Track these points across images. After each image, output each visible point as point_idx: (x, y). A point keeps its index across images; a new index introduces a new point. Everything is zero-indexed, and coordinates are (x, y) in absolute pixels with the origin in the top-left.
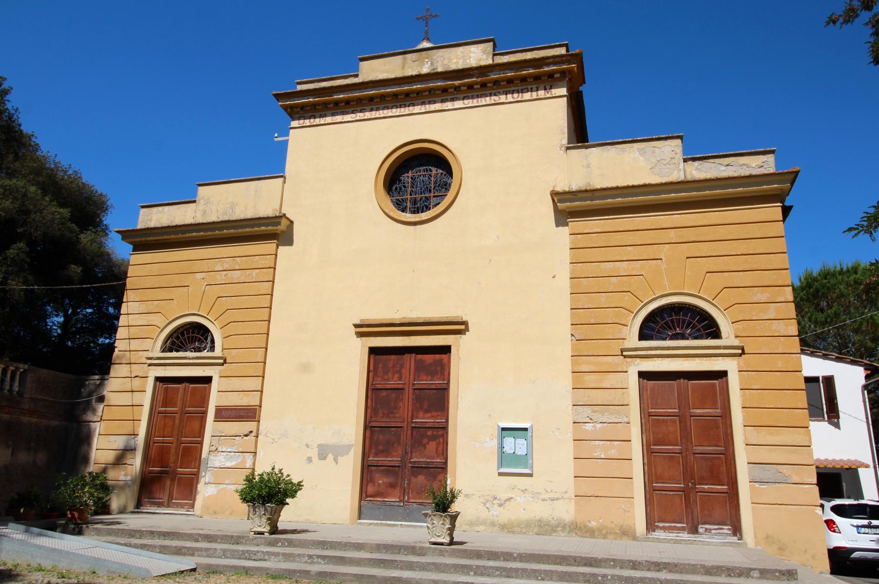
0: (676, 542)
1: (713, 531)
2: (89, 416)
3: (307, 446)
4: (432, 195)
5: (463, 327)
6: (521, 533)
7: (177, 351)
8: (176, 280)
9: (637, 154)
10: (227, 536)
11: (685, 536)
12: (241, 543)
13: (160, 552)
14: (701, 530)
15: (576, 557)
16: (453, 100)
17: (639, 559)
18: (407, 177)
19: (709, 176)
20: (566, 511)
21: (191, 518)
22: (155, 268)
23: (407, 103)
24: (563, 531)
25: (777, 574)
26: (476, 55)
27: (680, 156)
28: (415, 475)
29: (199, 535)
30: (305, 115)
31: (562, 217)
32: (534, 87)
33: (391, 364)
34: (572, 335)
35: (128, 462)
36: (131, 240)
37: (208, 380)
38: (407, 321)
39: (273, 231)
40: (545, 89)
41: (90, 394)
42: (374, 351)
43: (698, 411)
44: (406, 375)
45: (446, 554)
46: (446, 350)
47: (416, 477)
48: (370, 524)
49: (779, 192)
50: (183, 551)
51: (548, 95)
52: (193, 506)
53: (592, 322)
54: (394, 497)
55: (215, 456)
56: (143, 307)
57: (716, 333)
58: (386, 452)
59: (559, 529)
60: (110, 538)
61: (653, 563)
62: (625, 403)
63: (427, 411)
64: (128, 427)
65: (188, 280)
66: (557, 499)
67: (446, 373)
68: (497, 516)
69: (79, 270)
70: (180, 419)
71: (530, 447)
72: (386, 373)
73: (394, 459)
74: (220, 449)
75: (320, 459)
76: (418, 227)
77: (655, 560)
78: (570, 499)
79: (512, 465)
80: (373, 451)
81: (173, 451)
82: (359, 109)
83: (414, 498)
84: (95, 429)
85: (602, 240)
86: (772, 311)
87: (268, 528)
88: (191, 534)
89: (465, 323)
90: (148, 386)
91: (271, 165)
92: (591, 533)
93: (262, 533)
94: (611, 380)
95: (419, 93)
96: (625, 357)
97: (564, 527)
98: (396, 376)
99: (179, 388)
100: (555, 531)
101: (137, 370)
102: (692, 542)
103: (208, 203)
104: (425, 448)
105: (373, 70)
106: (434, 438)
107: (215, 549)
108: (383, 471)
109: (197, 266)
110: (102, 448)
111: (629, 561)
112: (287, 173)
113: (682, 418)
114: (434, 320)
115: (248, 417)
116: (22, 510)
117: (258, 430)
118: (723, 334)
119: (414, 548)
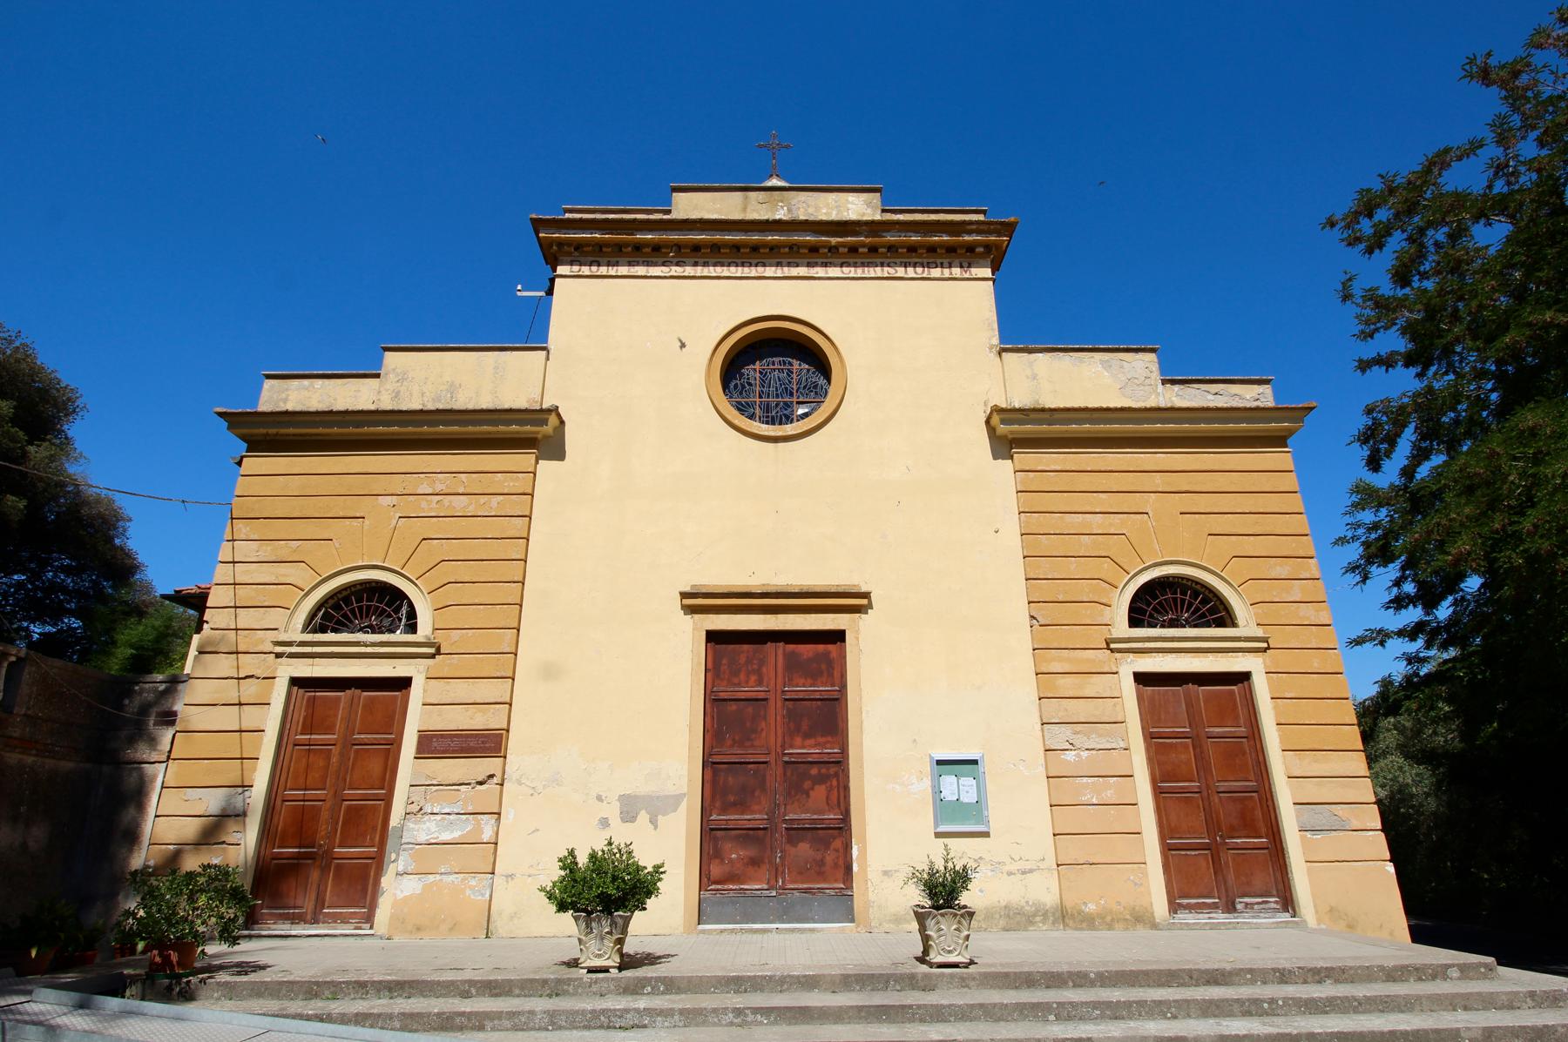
0: (1213, 927)
2: (143, 752)
3: (599, 798)
5: (864, 602)
7: (335, 631)
9: (1100, 368)
11: (1220, 917)
12: (566, 993)
13: (402, 1029)
14: (1239, 906)
16: (825, 265)
17: (1288, 966)
18: (753, 371)
20: (1044, 890)
21: (367, 941)
22: (295, 485)
24: (1044, 921)
26: (857, 207)
27: (1156, 376)
28: (792, 841)
29: (471, 983)
31: (1003, 446)
32: (946, 262)
34: (1033, 617)
35: (230, 839)
36: (245, 431)
37: (404, 683)
38: (773, 589)
39: (532, 433)
41: (144, 710)
42: (715, 638)
46: (838, 636)
47: (795, 845)
48: (722, 931)
52: (369, 919)
54: (759, 881)
55: (416, 823)
56: (267, 551)
58: (741, 805)
60: (273, 1005)
61: (1310, 970)
63: (807, 736)
64: (231, 772)
66: (1031, 871)
67: (836, 674)
69: (22, 504)
70: (341, 754)
73: (755, 817)
75: (624, 820)
76: (781, 445)
81: (325, 815)
83: (793, 882)
84: (155, 777)
85: (1062, 482)
86: (1297, 591)
88: (452, 983)
89: (866, 595)
90: (275, 694)
91: (529, 331)
92: (1089, 922)
93: (606, 970)
94: (1096, 685)
97: (1045, 915)
98: (753, 678)
99: (339, 698)
100: (1032, 923)
101: (249, 664)
102: (1235, 926)
103: (404, 379)
104: (808, 796)
105: (688, 206)
106: (822, 779)
107: (532, 1012)
108: (737, 837)
109: (379, 484)
110: (170, 813)
111: (1275, 970)
112: (551, 344)
114: (840, 590)
115: (485, 750)
116: (34, 953)
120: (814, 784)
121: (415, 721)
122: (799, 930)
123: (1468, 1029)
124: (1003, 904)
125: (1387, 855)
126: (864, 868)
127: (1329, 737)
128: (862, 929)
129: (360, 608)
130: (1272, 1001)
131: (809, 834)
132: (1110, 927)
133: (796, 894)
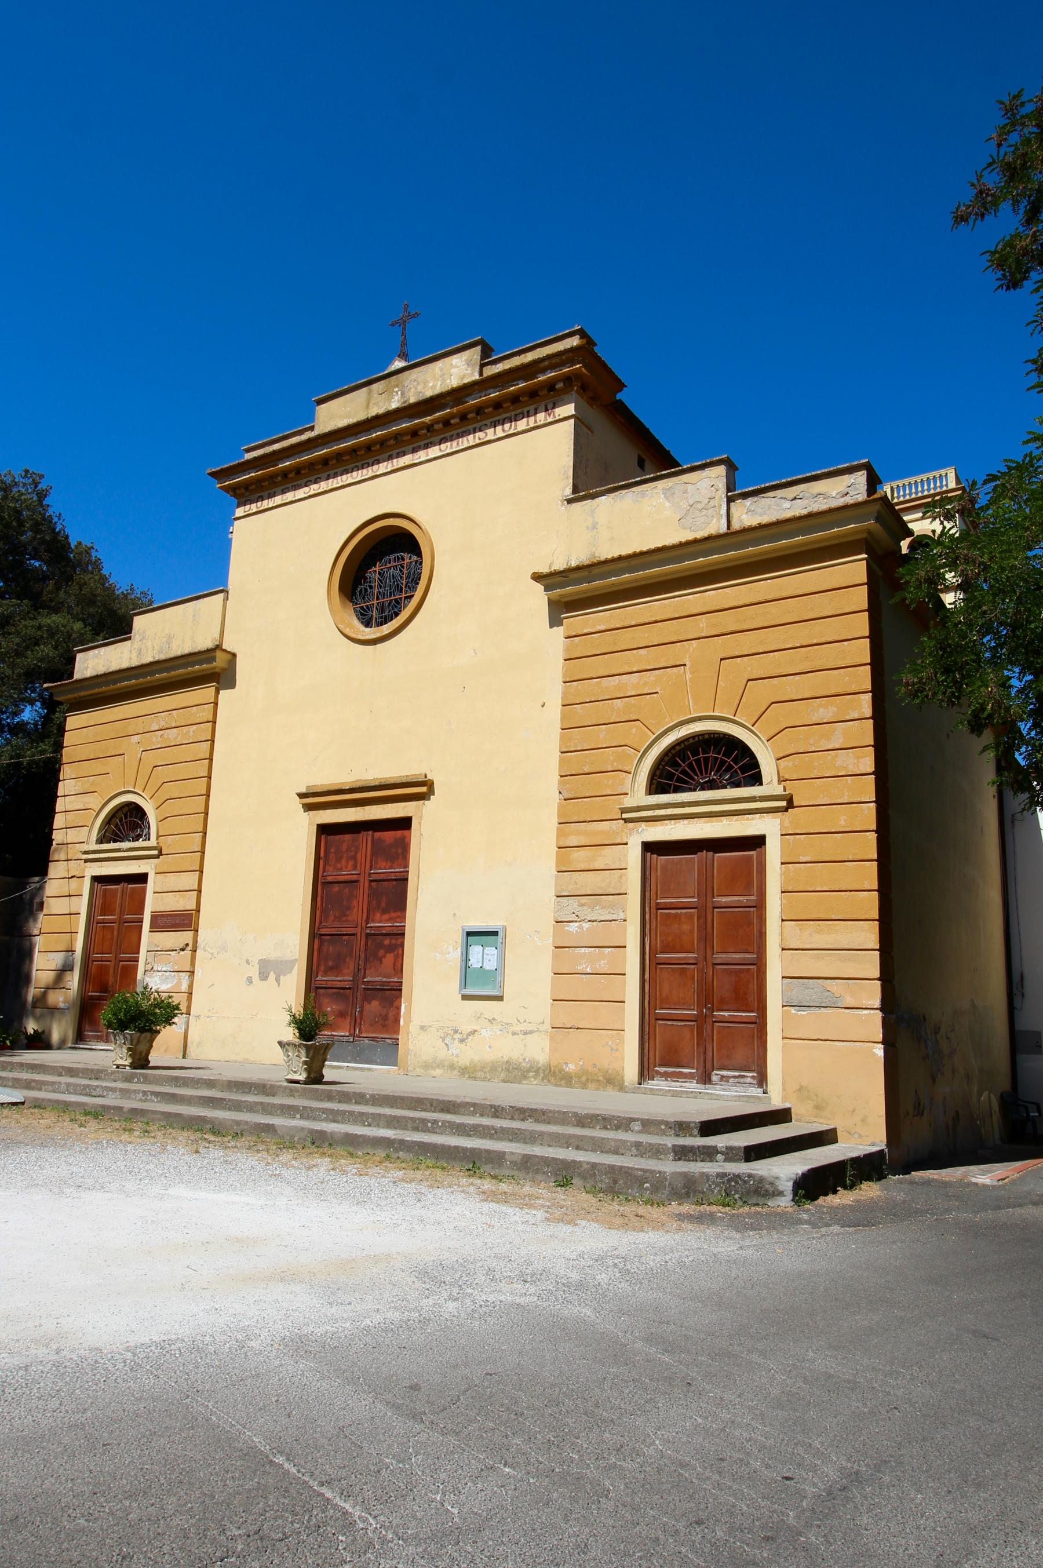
0: (675, 1094)
1: (731, 1080)
3: (248, 962)
4: (403, 595)
5: (424, 789)
6: (484, 1079)
8: (112, 747)
10: (88, 1069)
11: (692, 1086)
14: (714, 1078)
15: (432, 1100)
16: (427, 446)
17: (503, 1104)
18: (374, 573)
19: (765, 519)
20: (538, 1050)
23: (370, 461)
24: (535, 1077)
25: (663, 1127)
26: (458, 370)
28: (367, 999)
30: (251, 497)
32: (532, 408)
33: (344, 847)
37: (142, 878)
39: (207, 670)
40: (546, 410)
42: (324, 830)
43: (724, 899)
44: (358, 863)
45: (296, 1094)
46: (405, 823)
49: (865, 535)
50: (33, 1084)
51: (550, 420)
53: (586, 771)
54: (344, 1030)
57: (756, 779)
58: (335, 969)
59: (531, 1074)
62: (622, 891)
63: (385, 911)
65: (123, 746)
66: (531, 1032)
68: (457, 1056)
71: (502, 959)
72: (339, 860)
73: (344, 978)
74: (155, 968)
77: (520, 1105)
78: (546, 1032)
79: (479, 987)
80: (322, 968)
81: (111, 971)
82: (313, 478)
83: (367, 1032)
86: (838, 736)
87: (130, 1060)
91: (209, 577)
94: (607, 857)
95: (382, 442)
96: (626, 821)
97: (537, 1071)
98: (351, 863)
100: (525, 1077)
101: (75, 868)
104: (381, 962)
105: (333, 416)
110: (43, 965)
111: (492, 1106)
112: (231, 586)
113: (704, 910)
114: (392, 781)
117: (195, 941)
118: (765, 779)
119: (264, 1086)
120: (386, 953)
121: (151, 905)
122: (362, 1069)
123: (512, 1153)
124: (506, 1059)
125: (880, 1037)
126: (409, 1020)
127: (842, 904)
128: (402, 1072)
129: (698, 762)
130: (435, 1122)
131: (380, 993)
132: (584, 1086)
133: (367, 1041)
